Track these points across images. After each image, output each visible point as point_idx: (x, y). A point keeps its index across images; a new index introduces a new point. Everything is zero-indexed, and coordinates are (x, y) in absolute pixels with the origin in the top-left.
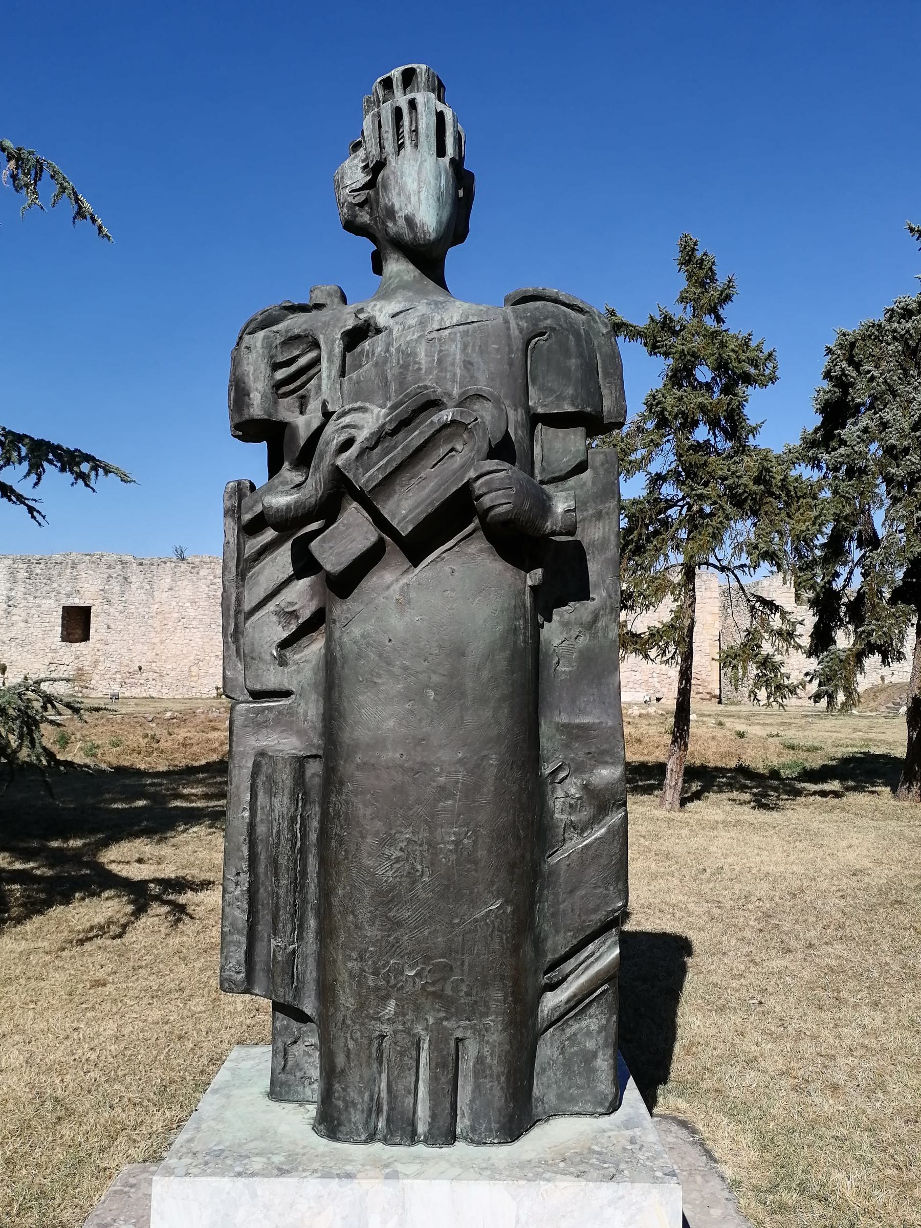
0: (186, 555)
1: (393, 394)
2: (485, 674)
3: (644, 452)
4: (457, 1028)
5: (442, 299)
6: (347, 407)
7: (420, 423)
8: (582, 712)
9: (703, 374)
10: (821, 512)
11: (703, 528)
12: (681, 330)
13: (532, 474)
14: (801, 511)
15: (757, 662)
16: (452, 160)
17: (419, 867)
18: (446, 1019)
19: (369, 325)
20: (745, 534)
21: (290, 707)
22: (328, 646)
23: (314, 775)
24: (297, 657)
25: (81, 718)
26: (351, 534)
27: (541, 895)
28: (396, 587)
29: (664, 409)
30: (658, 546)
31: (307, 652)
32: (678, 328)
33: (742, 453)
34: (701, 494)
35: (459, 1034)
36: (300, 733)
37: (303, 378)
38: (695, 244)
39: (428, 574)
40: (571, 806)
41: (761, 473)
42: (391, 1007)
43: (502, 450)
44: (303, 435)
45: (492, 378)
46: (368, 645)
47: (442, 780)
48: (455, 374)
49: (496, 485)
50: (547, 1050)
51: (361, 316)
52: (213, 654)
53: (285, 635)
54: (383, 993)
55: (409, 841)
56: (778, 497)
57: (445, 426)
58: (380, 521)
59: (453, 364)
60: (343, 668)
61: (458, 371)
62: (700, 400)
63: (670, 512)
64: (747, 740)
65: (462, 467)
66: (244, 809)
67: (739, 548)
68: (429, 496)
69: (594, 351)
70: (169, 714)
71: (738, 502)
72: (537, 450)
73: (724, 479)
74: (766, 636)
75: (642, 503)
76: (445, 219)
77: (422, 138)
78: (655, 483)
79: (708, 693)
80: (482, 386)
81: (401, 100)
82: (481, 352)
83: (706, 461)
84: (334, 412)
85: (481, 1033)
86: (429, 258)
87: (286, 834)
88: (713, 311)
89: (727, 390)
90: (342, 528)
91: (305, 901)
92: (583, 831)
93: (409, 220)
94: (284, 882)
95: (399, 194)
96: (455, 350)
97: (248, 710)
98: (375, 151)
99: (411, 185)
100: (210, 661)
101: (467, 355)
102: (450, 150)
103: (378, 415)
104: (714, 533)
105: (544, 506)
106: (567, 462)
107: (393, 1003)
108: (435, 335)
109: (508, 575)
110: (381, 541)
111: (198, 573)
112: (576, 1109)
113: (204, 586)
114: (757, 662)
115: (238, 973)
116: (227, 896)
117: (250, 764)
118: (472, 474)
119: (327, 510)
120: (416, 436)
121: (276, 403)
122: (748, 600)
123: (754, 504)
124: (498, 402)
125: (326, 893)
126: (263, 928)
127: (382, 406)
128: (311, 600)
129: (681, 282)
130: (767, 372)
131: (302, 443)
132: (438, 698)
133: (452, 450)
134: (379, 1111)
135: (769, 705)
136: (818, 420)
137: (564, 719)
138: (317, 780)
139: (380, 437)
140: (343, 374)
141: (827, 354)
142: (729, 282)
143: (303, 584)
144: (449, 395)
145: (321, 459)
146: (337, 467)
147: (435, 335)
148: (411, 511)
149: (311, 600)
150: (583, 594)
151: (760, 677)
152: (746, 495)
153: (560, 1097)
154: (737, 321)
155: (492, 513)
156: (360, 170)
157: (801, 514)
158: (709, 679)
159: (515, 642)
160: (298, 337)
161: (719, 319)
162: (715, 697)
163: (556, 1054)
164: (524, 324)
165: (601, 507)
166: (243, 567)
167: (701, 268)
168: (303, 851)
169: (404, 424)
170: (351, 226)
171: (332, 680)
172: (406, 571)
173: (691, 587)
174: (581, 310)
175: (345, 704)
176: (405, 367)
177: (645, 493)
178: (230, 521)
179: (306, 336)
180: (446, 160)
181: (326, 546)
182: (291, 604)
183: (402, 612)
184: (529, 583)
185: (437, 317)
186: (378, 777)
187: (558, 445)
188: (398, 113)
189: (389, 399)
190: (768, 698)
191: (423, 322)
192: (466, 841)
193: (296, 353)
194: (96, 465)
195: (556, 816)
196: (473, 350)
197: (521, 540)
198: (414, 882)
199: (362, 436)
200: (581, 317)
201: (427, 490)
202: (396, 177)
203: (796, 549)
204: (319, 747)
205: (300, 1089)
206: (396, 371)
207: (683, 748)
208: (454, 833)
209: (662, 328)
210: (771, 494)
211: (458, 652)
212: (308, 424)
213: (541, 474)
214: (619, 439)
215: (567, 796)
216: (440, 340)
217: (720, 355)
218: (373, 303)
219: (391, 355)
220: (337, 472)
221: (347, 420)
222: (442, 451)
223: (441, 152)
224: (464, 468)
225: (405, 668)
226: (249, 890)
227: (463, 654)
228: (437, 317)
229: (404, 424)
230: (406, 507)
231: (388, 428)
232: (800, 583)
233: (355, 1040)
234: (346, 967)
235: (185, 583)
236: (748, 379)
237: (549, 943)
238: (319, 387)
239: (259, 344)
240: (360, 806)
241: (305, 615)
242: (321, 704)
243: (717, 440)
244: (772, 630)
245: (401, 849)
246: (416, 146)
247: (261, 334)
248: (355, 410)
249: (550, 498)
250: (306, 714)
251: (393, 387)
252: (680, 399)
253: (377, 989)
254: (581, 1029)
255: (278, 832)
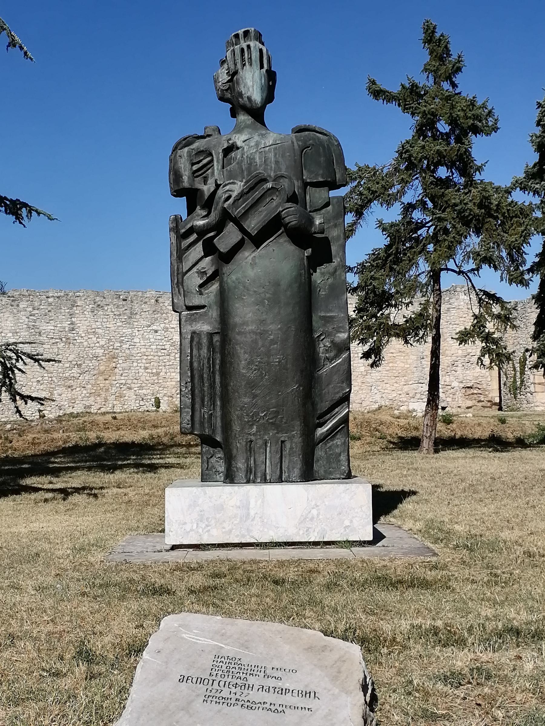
0: (6, 289)
1: (245, 176)
2: (289, 293)
3: (399, 187)
4: (283, 436)
5: (264, 132)
6: (227, 182)
7: (259, 189)
8: (331, 311)
9: (443, 127)
10: (526, 228)
11: (445, 243)
12: (425, 94)
13: (306, 209)
14: (514, 227)
15: (482, 337)
16: (267, 71)
17: (264, 372)
18: (277, 433)
19: (234, 146)
20: (472, 245)
21: (205, 312)
22: (221, 286)
23: (217, 341)
24: (206, 291)
25: (40, 365)
26: (230, 236)
27: (315, 386)
28: (250, 258)
29: (411, 156)
30: (411, 257)
31: (210, 289)
32: (422, 93)
33: (470, 186)
34: (439, 217)
35: (282, 439)
36: (210, 323)
37: (205, 169)
38: (435, 28)
39: (263, 252)
40: (326, 350)
41: (482, 201)
42: (254, 429)
43: (293, 198)
44: (207, 194)
45: (287, 168)
46: (239, 283)
47: (272, 337)
48: (271, 167)
49: (291, 213)
50: (319, 452)
51: (230, 142)
52: (35, 380)
53: (202, 282)
54: (251, 423)
55: (259, 362)
56: (496, 218)
57: (269, 189)
58: (242, 230)
59: (271, 162)
60: (228, 293)
61: (273, 165)
62: (438, 147)
63: (419, 232)
64: (508, 425)
65: (276, 206)
66: (188, 356)
67: (467, 256)
68: (263, 218)
69: (331, 153)
70: (9, 426)
71: (466, 223)
72: (308, 197)
73: (455, 205)
74: (489, 319)
75: (398, 225)
76: (264, 97)
77: (253, 62)
78: (408, 211)
79: (489, 401)
80: (283, 172)
81: (244, 45)
82: (282, 157)
83: (443, 193)
84: (221, 185)
85: (291, 438)
86: (257, 114)
87: (206, 365)
88: (449, 78)
89: (458, 140)
90: (227, 233)
91: (215, 394)
92: (332, 361)
93: (249, 98)
94: (206, 385)
95: (244, 87)
96: (271, 155)
97: (187, 314)
98: (232, 67)
99: (250, 83)
100: (32, 386)
101: (276, 158)
102: (265, 66)
103: (240, 186)
104: (449, 246)
105: (311, 221)
106: (321, 202)
107: (255, 427)
108: (262, 150)
109: (297, 251)
110: (243, 238)
111: (18, 306)
112: (332, 477)
113: (24, 318)
114: (482, 337)
115: (188, 424)
116: (182, 393)
117: (189, 337)
118: (281, 209)
119: (218, 227)
120: (257, 194)
121: (194, 180)
122: (477, 295)
123: (478, 223)
124: (290, 179)
125: (225, 386)
126: (197, 406)
127: (242, 181)
128: (212, 266)
129: (425, 57)
130: (490, 124)
131: (206, 198)
132: (269, 304)
133: (272, 199)
134: (251, 472)
135: (491, 368)
136: (535, 157)
137: (323, 314)
138: (218, 344)
139: (242, 195)
140: (223, 168)
141: (538, 108)
142: (459, 57)
143: (208, 259)
144: (270, 176)
145: (217, 204)
146: (225, 208)
147: (262, 150)
148: (255, 226)
149: (212, 266)
150: (330, 261)
151: (484, 348)
152: (471, 217)
153: (325, 472)
154: (468, 85)
155: (289, 225)
156: (225, 74)
157: (514, 229)
158: (489, 388)
159: (301, 280)
160: (203, 151)
161: (454, 85)
162: (495, 404)
163: (323, 454)
164: (300, 143)
165: (336, 222)
166: (180, 254)
167: (439, 46)
168: (214, 372)
169: (252, 189)
170: (222, 99)
171: (223, 300)
172: (254, 251)
173: (438, 287)
174: (325, 135)
175: (230, 308)
176: (250, 164)
177: (400, 218)
178: (172, 233)
179: (206, 151)
180: (264, 70)
181: (221, 241)
182: (203, 268)
183: (253, 268)
184: (306, 255)
185: (263, 142)
186: (245, 337)
187: (317, 195)
188: (242, 50)
189: (244, 178)
190: (491, 363)
191: (257, 144)
192: (283, 361)
193: (202, 158)
194: (30, 210)
195: (320, 355)
196: (279, 156)
197: (301, 236)
198: (262, 378)
199: (234, 194)
200: (325, 138)
201: (262, 216)
202: (243, 80)
203: (509, 254)
204: (218, 328)
205: (215, 476)
206: (247, 166)
207: (434, 408)
208: (278, 358)
209: (411, 93)
210: (492, 216)
211: (277, 284)
212: (209, 189)
213: (310, 208)
214: (380, 178)
215: (325, 346)
216: (265, 152)
217: (451, 114)
218: (234, 135)
219: (244, 159)
220: (224, 210)
221: (227, 188)
222: (268, 200)
223: (262, 67)
224: (277, 207)
225: (255, 292)
226: (191, 389)
227: (279, 285)
228: (263, 142)
229: (252, 189)
230: (253, 224)
231: (245, 191)
232: (512, 279)
233: (240, 443)
234: (235, 414)
235: (7, 315)
236: (476, 131)
237: (319, 406)
238: (213, 173)
239: (185, 155)
240: (239, 349)
241: (210, 273)
242: (219, 311)
243: (454, 176)
244: (494, 315)
245: (256, 366)
246: (251, 65)
247: (186, 149)
248: (230, 183)
249: (313, 218)
250: (212, 315)
251: (245, 173)
252: (423, 147)
253: (249, 421)
254: (333, 444)
255: (203, 364)
